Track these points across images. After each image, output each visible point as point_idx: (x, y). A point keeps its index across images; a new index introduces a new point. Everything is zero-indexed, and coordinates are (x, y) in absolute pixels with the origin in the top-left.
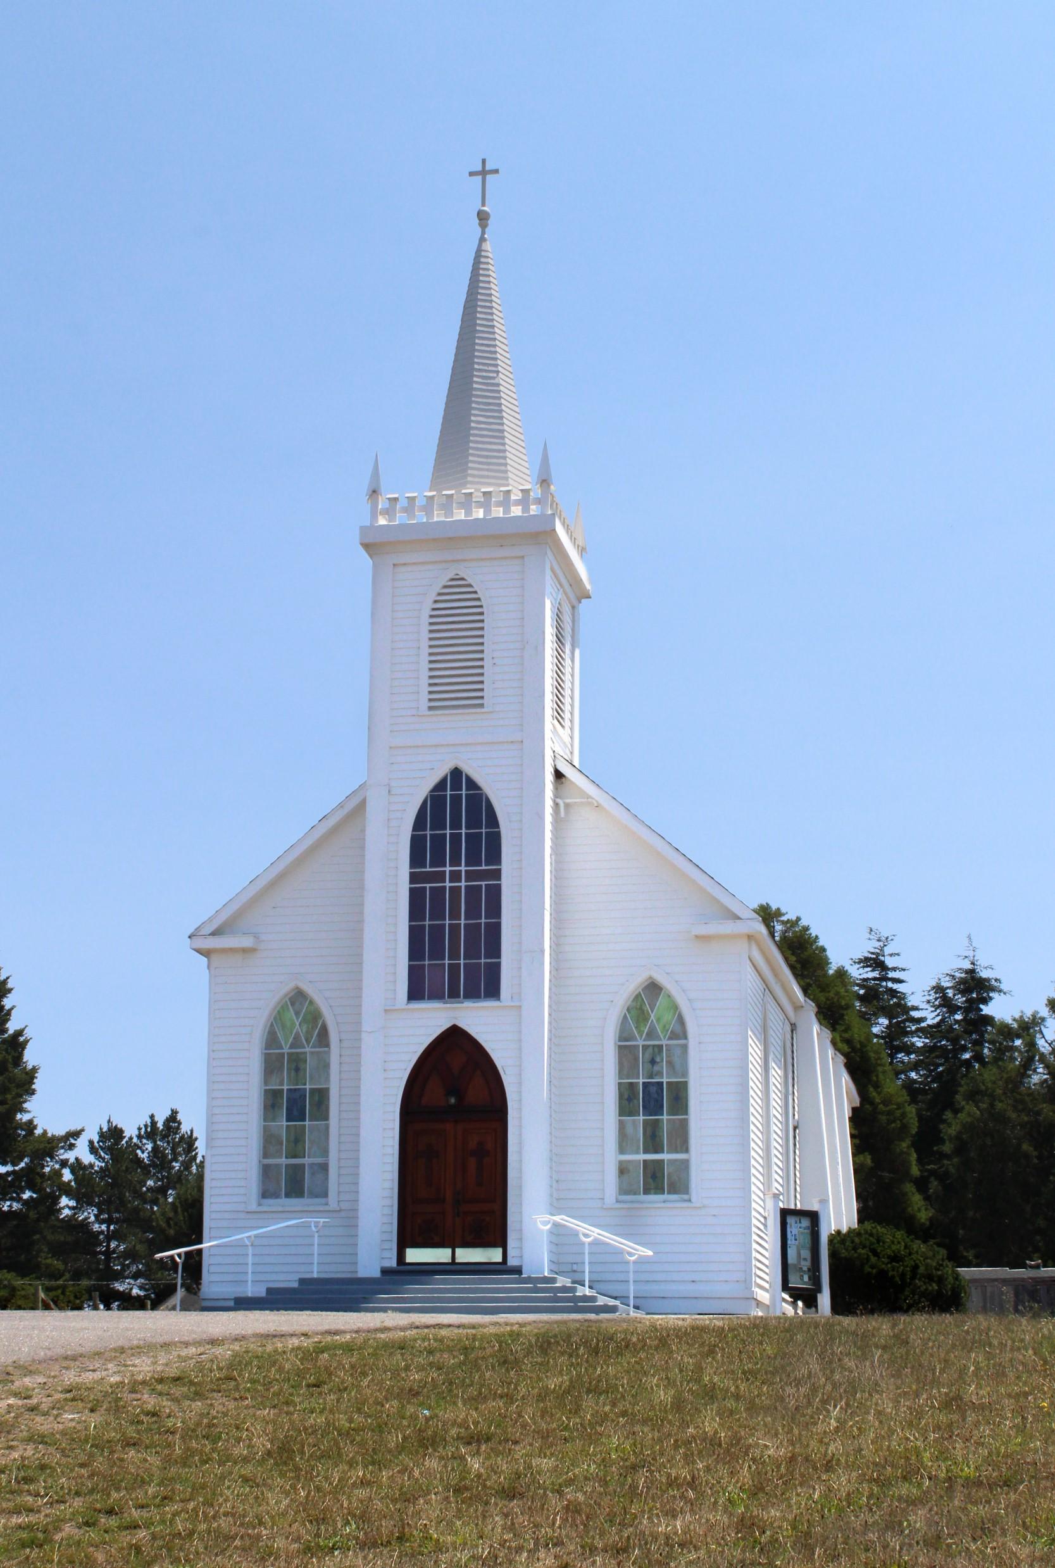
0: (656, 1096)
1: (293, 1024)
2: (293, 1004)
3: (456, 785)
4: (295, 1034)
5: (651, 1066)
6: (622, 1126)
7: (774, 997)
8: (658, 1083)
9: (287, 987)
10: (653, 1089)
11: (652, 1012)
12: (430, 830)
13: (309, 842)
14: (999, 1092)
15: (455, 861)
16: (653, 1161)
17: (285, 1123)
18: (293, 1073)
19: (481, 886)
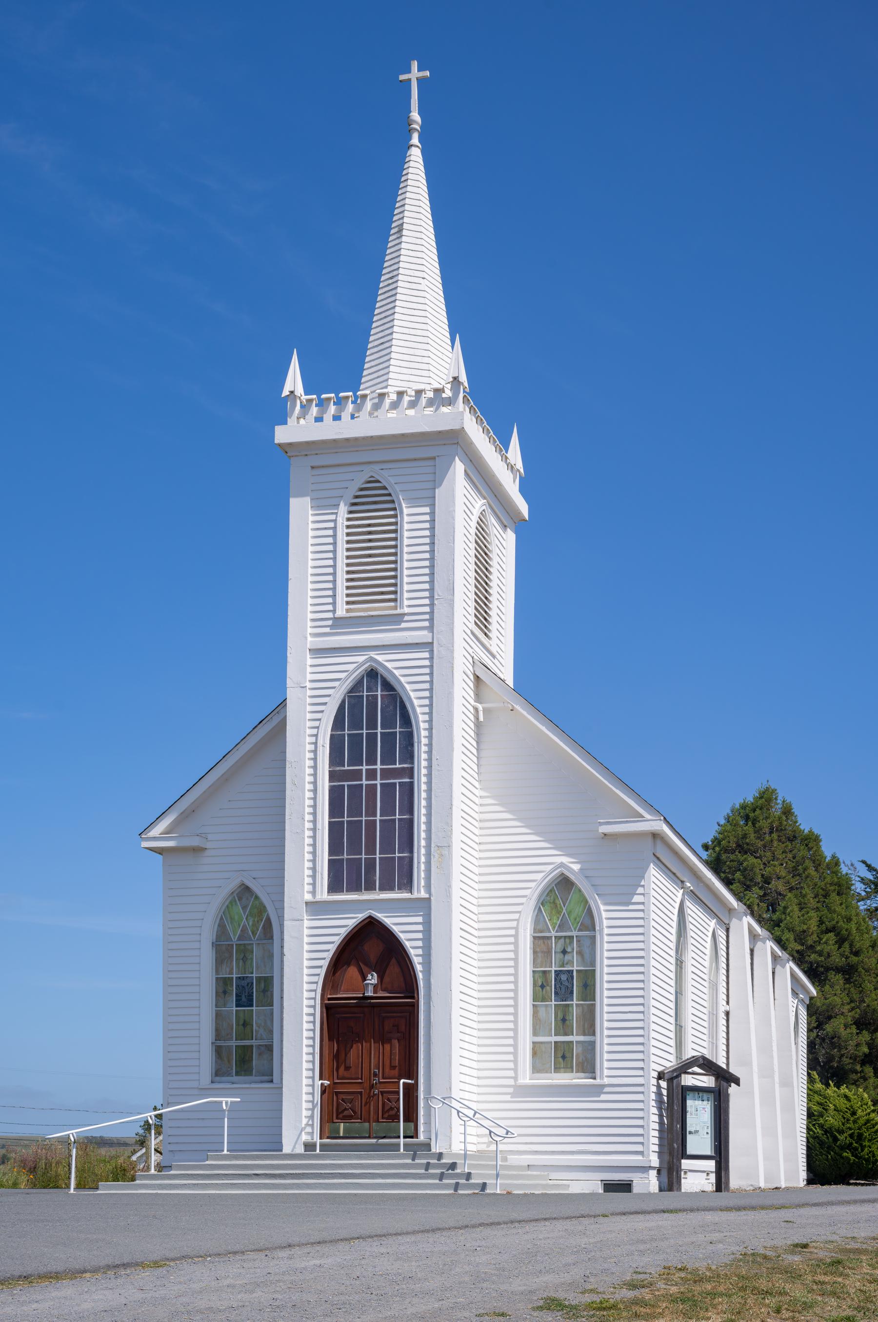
2: (240, 899)
4: (243, 927)
9: (233, 885)
10: (564, 977)
14: (815, 1278)
15: (372, 760)
17: (235, 1009)
18: (241, 962)
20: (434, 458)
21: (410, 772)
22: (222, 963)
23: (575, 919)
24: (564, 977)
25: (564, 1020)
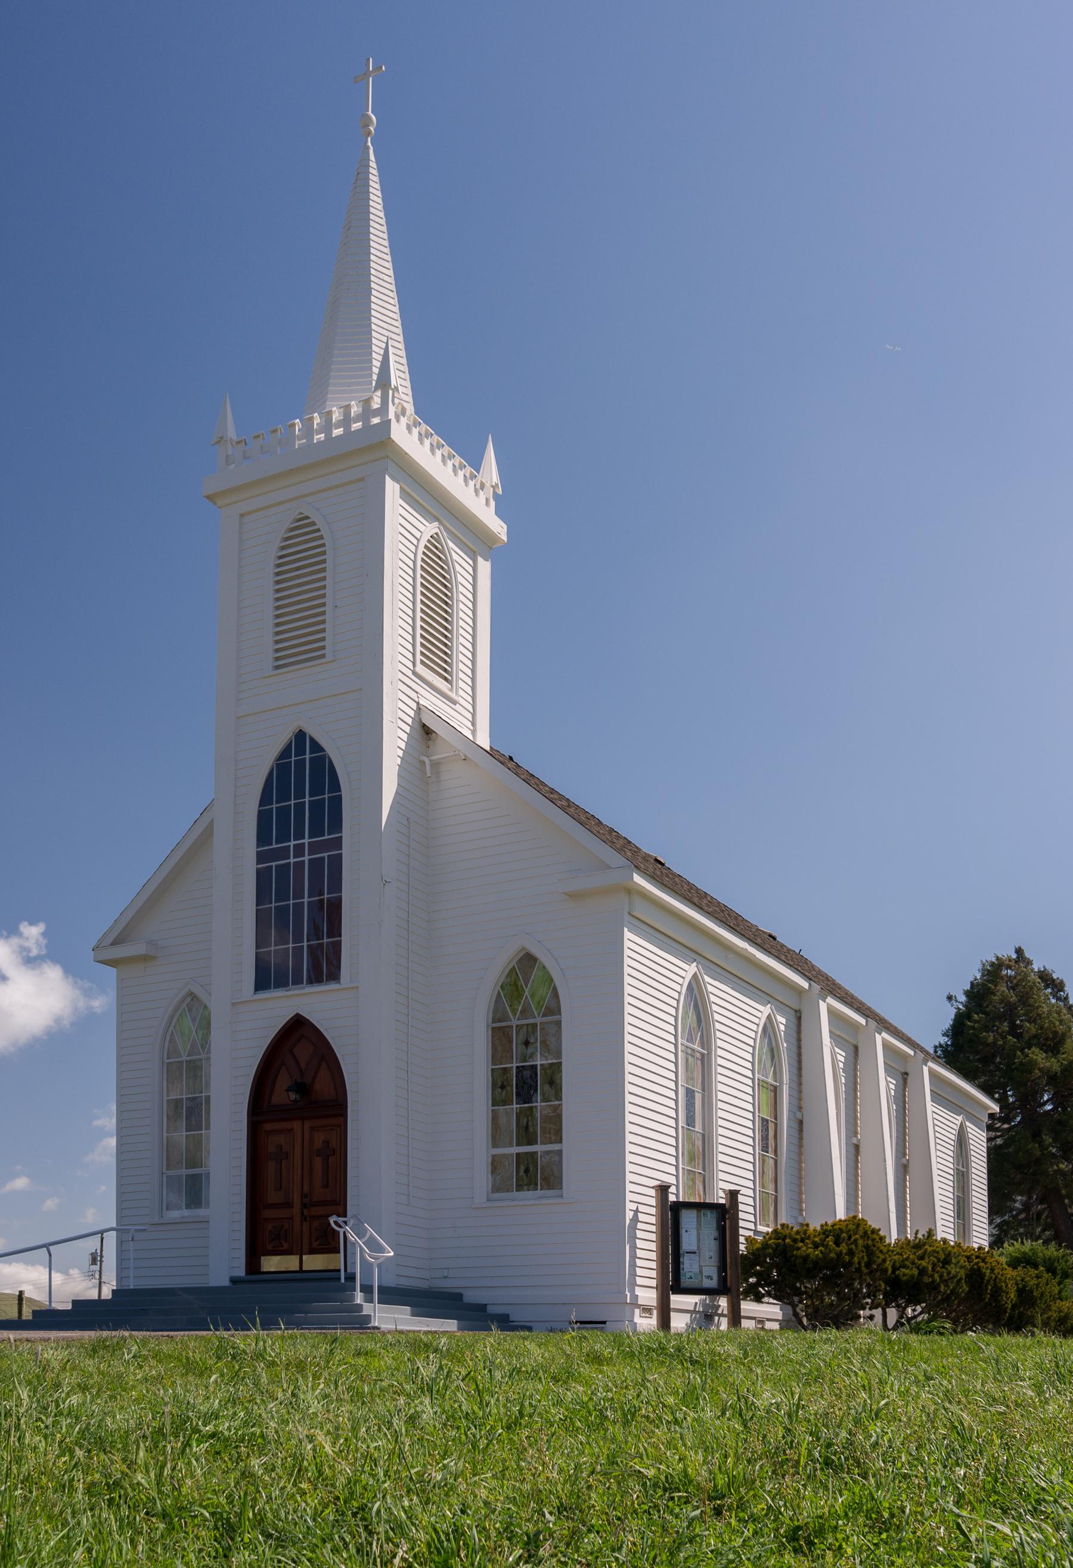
3: (301, 751)
4: (192, 1041)
5: (525, 1047)
6: (495, 1118)
7: (744, 980)
13: (190, 841)
15: (300, 835)
17: (185, 1133)
20: (362, 479)
23: (539, 1003)
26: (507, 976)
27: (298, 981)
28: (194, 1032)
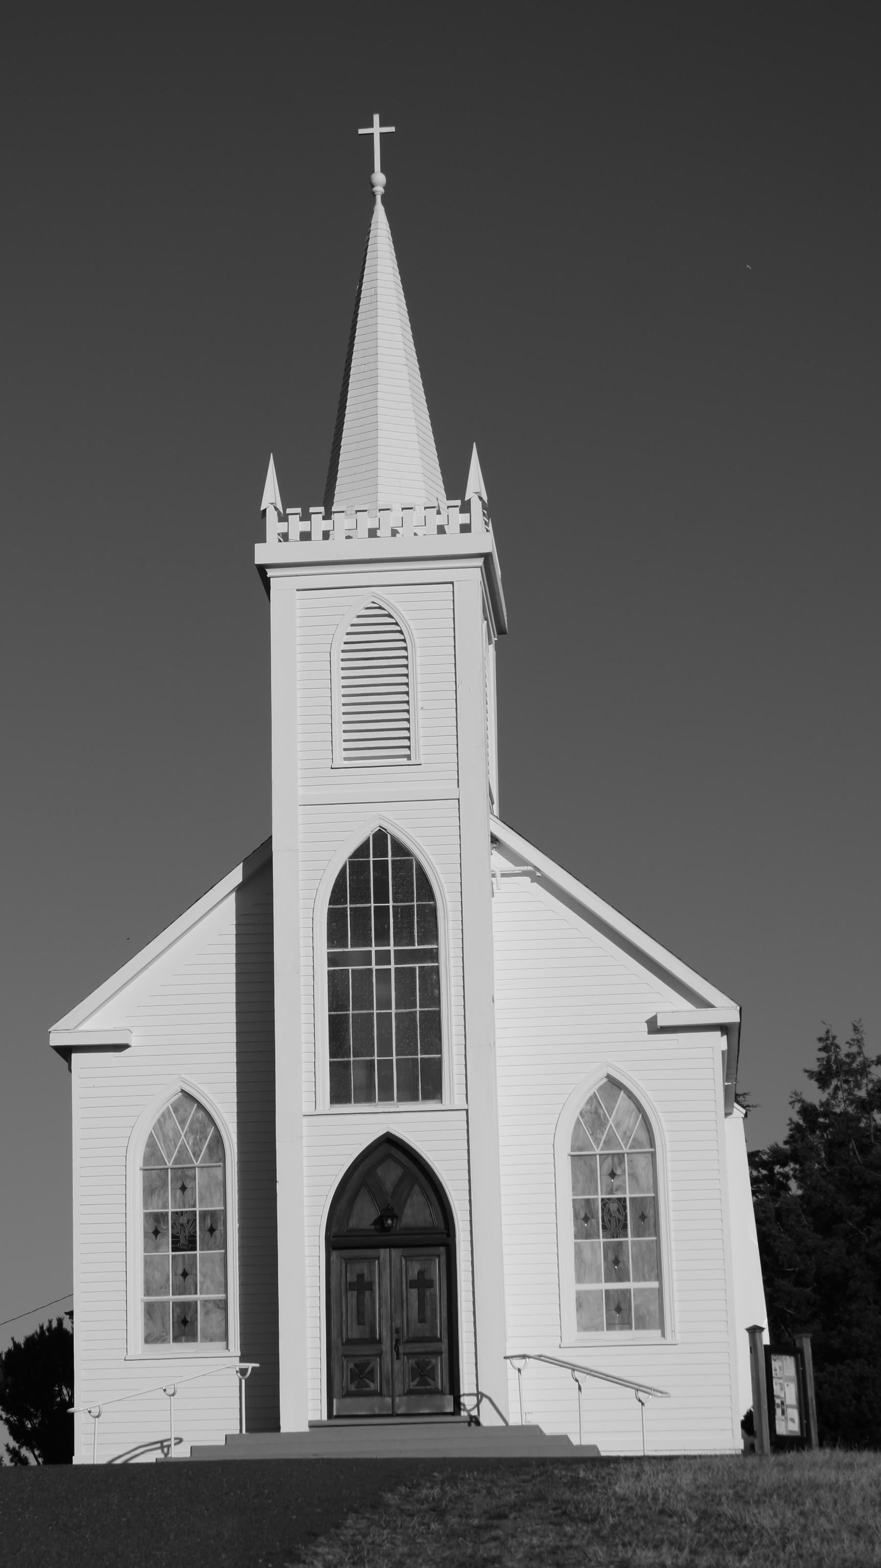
0: (617, 1215)
1: (177, 1135)
2: (176, 1110)
3: (381, 850)
4: (180, 1146)
8: (619, 1199)
10: (613, 1207)
11: (610, 1117)
12: (413, 906)
15: (382, 938)
16: (617, 1291)
17: (171, 1253)
18: (179, 1192)
19: (348, 970)
21: (433, 955)
22: (152, 1194)
24: (613, 1207)
25: (616, 1262)
26: (588, 1102)
27: (386, 1096)
28: (183, 1137)
